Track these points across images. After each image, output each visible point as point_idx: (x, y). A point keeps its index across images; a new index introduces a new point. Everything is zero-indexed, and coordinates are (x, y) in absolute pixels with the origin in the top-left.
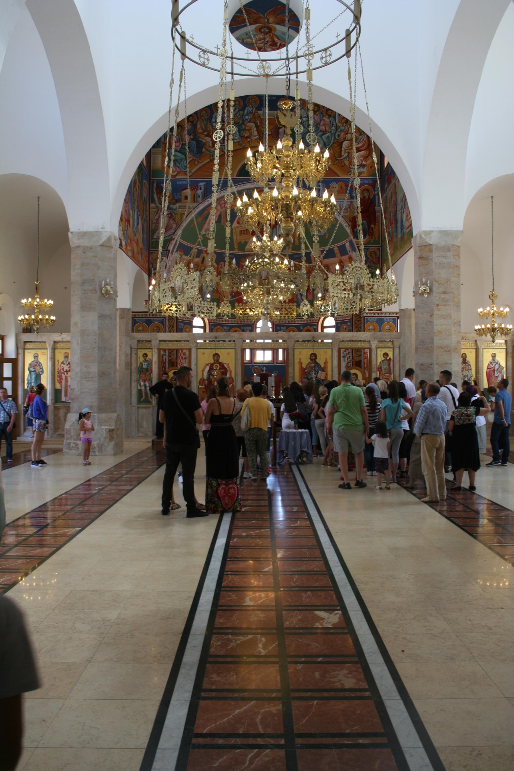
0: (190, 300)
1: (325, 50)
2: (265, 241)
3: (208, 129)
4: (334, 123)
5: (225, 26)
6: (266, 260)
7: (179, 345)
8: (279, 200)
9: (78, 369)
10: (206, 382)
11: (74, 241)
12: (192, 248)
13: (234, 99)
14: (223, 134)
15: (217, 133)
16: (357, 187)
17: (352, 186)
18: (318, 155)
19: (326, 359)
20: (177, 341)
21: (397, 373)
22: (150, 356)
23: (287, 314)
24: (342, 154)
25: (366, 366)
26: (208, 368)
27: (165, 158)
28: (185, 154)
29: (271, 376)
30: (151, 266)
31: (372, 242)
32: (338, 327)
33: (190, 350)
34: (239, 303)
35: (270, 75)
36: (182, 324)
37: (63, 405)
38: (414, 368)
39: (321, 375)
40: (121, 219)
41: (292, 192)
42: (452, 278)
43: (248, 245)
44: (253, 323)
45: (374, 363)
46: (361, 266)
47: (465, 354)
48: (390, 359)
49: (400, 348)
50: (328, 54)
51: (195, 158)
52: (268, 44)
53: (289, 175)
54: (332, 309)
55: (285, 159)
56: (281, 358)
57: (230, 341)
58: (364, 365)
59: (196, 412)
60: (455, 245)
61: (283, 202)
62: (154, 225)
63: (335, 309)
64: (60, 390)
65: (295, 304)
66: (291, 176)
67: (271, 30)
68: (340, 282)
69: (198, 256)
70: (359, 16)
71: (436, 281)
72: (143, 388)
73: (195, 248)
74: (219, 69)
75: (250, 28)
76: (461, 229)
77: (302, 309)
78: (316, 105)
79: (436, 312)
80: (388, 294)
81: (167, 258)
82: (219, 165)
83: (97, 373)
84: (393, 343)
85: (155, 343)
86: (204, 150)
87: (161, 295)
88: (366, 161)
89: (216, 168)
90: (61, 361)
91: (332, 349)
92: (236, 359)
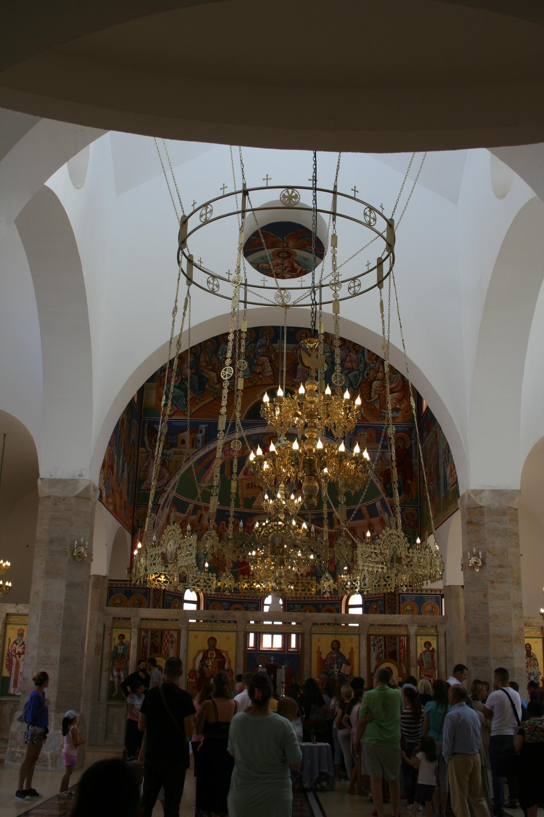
0: (185, 569)
1: (354, 279)
2: (279, 499)
3: (213, 363)
4: (363, 360)
5: (240, 251)
6: (280, 523)
7: (166, 625)
8: (300, 455)
9: (35, 653)
10: (198, 675)
11: (43, 490)
12: (188, 504)
13: (246, 330)
14: (233, 371)
15: (225, 370)
16: (392, 436)
17: (386, 434)
18: (348, 401)
19: (352, 648)
20: (162, 620)
21: (443, 669)
22: (127, 638)
23: (304, 590)
24: (372, 396)
25: (402, 658)
26: (201, 656)
27: (162, 396)
28: (185, 391)
29: (281, 668)
30: (135, 523)
31: (408, 501)
32: (365, 606)
33: (179, 632)
34: (244, 575)
35: (289, 306)
36: (170, 598)
37: (10, 698)
38: (464, 663)
39: (345, 669)
40: (103, 466)
41: (316, 444)
42: (509, 549)
43: (256, 502)
44: (259, 599)
45: (413, 654)
46: (398, 534)
47: (529, 645)
48: (433, 648)
49: (445, 636)
50: (356, 284)
51: (196, 396)
52: (287, 270)
53: (313, 425)
54: (360, 586)
55: (309, 406)
56: (293, 645)
57: (229, 622)
58: (400, 656)
59: (186, 719)
60: (512, 508)
61: (305, 457)
62: (142, 474)
63: (365, 585)
64: (8, 679)
65: (314, 578)
66: (315, 426)
67: (291, 255)
68: (372, 552)
69: (194, 513)
70: (392, 244)
71: (489, 552)
72: (116, 679)
73: (192, 503)
74: (231, 297)
75: (267, 252)
76: (518, 488)
77: (323, 584)
78: (341, 339)
79: (490, 591)
80: (431, 569)
81: (156, 514)
82: (227, 406)
83: (59, 659)
84: (436, 630)
85: (135, 621)
86: (207, 386)
87: (148, 563)
88: (401, 405)
89: (223, 410)
90: (13, 640)
91: (359, 635)
92: (237, 646)
